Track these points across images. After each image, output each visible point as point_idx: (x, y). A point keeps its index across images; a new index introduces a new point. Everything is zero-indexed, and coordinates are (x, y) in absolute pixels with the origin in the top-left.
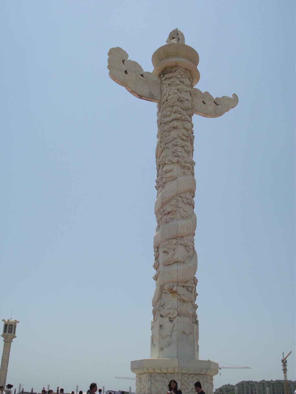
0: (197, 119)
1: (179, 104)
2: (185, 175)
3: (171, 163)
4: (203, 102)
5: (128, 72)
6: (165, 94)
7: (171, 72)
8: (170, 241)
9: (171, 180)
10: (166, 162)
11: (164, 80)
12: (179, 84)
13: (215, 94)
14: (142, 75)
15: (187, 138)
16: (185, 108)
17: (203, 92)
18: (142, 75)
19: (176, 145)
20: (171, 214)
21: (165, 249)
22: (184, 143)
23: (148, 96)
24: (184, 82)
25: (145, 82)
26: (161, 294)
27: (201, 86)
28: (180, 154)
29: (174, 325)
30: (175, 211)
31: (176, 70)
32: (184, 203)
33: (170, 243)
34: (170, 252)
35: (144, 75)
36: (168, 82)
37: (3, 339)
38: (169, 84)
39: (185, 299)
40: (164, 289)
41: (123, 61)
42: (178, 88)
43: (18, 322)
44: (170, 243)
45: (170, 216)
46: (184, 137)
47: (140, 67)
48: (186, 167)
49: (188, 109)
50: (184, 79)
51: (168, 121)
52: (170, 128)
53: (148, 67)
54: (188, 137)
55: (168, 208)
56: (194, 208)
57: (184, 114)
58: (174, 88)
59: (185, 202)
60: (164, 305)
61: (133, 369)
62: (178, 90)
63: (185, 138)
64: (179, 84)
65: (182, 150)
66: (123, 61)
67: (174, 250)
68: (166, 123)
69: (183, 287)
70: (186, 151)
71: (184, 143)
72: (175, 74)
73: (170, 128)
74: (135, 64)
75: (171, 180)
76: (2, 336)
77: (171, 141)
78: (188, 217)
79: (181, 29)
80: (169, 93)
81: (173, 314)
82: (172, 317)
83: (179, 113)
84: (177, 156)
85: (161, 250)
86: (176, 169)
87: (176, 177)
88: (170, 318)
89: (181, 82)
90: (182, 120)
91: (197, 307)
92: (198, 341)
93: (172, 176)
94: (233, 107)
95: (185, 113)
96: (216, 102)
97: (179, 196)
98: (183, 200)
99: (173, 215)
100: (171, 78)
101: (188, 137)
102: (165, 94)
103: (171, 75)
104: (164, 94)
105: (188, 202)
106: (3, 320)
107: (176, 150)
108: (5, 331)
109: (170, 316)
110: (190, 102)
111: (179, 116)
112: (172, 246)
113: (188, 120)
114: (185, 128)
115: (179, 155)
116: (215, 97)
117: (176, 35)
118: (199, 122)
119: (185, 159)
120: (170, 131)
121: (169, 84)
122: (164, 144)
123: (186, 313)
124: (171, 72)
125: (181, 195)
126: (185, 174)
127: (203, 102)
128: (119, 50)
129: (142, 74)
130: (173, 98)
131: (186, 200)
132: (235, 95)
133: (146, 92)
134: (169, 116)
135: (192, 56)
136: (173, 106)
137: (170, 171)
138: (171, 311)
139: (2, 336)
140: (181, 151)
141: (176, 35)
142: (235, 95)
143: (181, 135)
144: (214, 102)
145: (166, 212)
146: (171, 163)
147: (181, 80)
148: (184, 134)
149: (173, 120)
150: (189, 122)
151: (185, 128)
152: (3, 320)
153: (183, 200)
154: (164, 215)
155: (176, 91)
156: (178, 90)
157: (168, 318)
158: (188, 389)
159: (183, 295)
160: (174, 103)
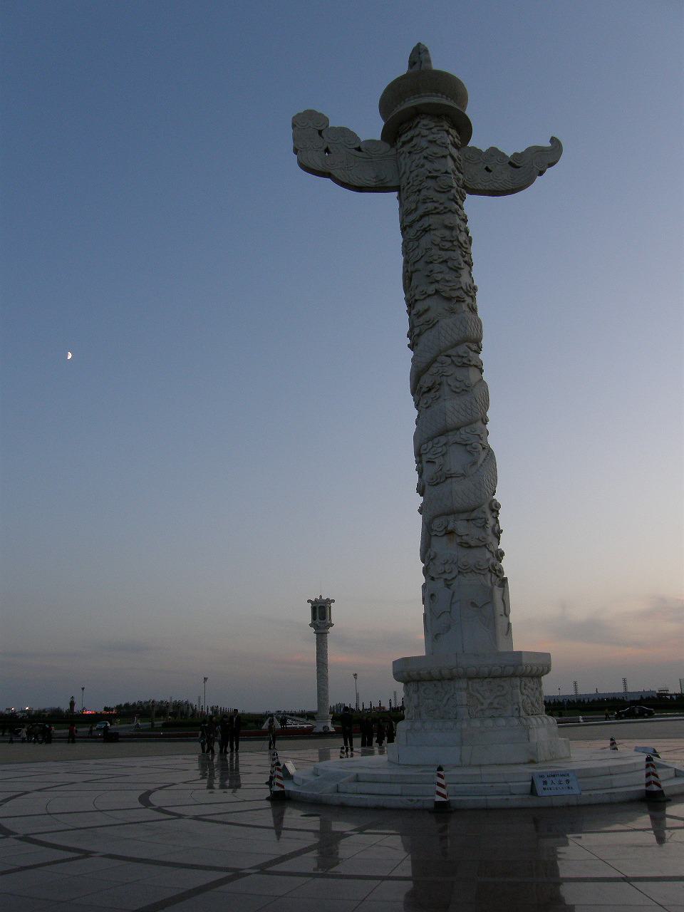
0: (474, 206)
1: (430, 183)
2: (454, 313)
3: (425, 298)
4: (487, 169)
5: (331, 150)
6: (404, 173)
7: (411, 128)
8: (436, 440)
9: (429, 328)
10: (417, 297)
11: (402, 147)
12: (427, 148)
13: (510, 148)
14: (359, 149)
15: (450, 244)
16: (442, 190)
17: (484, 151)
18: (359, 149)
19: (431, 262)
20: (433, 391)
21: (429, 456)
22: (445, 255)
23: (374, 184)
24: (435, 141)
25: (365, 160)
26: (430, 540)
27: (480, 140)
28: (439, 277)
29: (454, 592)
30: (439, 384)
31: (419, 122)
32: (456, 365)
33: (437, 444)
34: (436, 460)
35: (362, 147)
36: (406, 149)
37: (313, 630)
38: (410, 153)
39: (473, 543)
40: (432, 530)
41: (320, 132)
42: (426, 155)
43: (333, 601)
44: (437, 444)
45: (432, 394)
46: (444, 243)
47: (353, 135)
48: (454, 298)
49: (449, 189)
50: (435, 136)
51: (414, 221)
52: (419, 233)
53: (370, 127)
54: (452, 241)
55: (427, 381)
56: (481, 371)
57: (441, 202)
58: (417, 157)
59: (457, 364)
60: (434, 558)
61: (398, 676)
62: (426, 158)
63: (448, 245)
64: (427, 148)
65: (443, 267)
66: (320, 132)
67: (443, 455)
68: (410, 226)
69: (468, 520)
70: (451, 269)
71: (445, 255)
72: (416, 131)
73: (419, 233)
74: (344, 132)
75: (429, 328)
76: (311, 625)
77: (422, 257)
78: (466, 391)
79: (426, 43)
80: (410, 168)
81: (451, 572)
82: (448, 577)
83: (430, 202)
84: (434, 281)
85: (425, 458)
86: (436, 306)
87: (436, 321)
88: (446, 580)
89: (430, 142)
90: (438, 213)
91: (502, 554)
92: (507, 615)
93: (428, 319)
94: (551, 165)
95: (443, 198)
96: (514, 163)
97: (446, 354)
98: (453, 361)
99: (437, 391)
100: (412, 139)
101: (452, 241)
102: (404, 173)
103: (410, 134)
104: (402, 171)
105: (464, 363)
106: (309, 601)
107: (432, 271)
108: (314, 618)
109: (446, 576)
110: (452, 176)
111: (430, 206)
112: (440, 450)
113: (450, 211)
114: (446, 227)
115: (437, 279)
116: (509, 153)
117: (419, 55)
118: (479, 212)
119: (451, 284)
120: (418, 239)
121: (410, 153)
122: (411, 266)
123: (475, 567)
124: (411, 128)
125: (449, 352)
126: (452, 312)
127: (487, 169)
128: (311, 114)
129: (357, 146)
130: (417, 176)
131: (460, 360)
132: (553, 140)
133: (368, 178)
134: (416, 209)
135: (450, 87)
136: (419, 191)
137: (426, 311)
138: (447, 567)
139: (311, 625)
140: (441, 270)
141: (419, 55)
142: (553, 140)
143: (438, 240)
144: (510, 163)
145: (424, 389)
146: (425, 298)
147: (431, 137)
148: (444, 237)
149: (422, 217)
150: (453, 213)
151: (446, 227)
152: (309, 601)
153: (453, 361)
154: (422, 395)
155: (422, 161)
156: (426, 158)
157: (442, 580)
158: (482, 704)
159: (467, 535)
160: (420, 184)
